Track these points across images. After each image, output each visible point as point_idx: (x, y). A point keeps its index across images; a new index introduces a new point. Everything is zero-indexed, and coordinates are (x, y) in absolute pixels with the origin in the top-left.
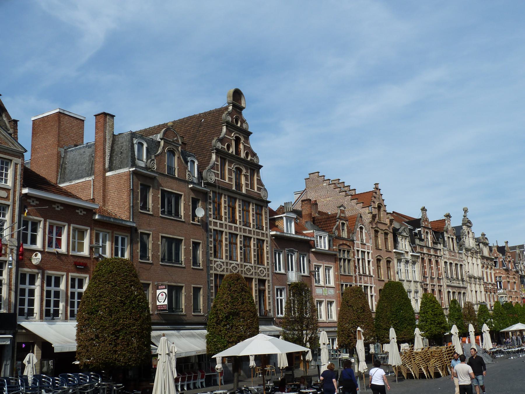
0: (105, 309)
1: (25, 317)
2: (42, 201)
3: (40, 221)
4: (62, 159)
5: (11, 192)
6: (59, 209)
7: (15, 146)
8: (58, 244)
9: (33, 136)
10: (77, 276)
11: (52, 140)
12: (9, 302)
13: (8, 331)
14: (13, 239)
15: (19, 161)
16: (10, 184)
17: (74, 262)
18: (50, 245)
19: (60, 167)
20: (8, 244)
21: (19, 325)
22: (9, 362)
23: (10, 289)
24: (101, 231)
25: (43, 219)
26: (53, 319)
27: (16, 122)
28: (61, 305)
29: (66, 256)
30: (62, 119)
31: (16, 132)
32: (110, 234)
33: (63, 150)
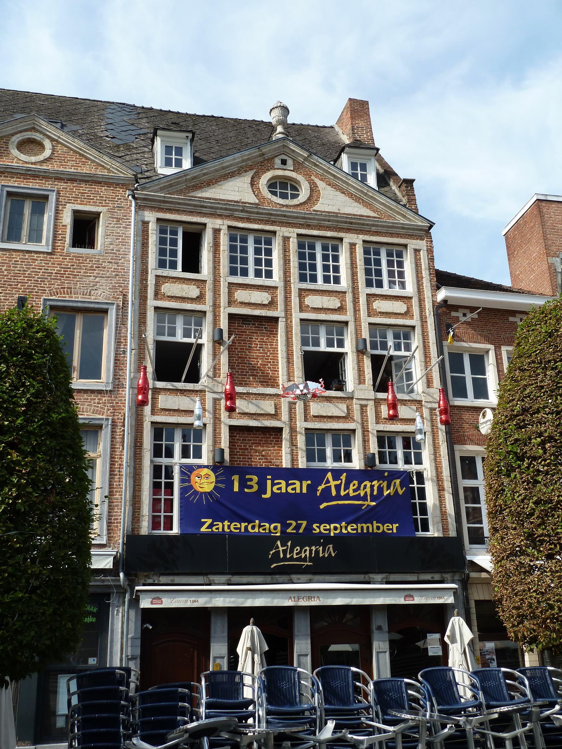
0: (543, 443)
3: (487, 352)
5: (415, 302)
7: (410, 220)
9: (509, 259)
11: (536, 249)
12: (443, 514)
13: (448, 576)
14: (431, 390)
15: (422, 244)
20: (423, 399)
21: (472, 563)
23: (441, 489)
27: (409, 183)
30: (545, 210)
31: (412, 199)
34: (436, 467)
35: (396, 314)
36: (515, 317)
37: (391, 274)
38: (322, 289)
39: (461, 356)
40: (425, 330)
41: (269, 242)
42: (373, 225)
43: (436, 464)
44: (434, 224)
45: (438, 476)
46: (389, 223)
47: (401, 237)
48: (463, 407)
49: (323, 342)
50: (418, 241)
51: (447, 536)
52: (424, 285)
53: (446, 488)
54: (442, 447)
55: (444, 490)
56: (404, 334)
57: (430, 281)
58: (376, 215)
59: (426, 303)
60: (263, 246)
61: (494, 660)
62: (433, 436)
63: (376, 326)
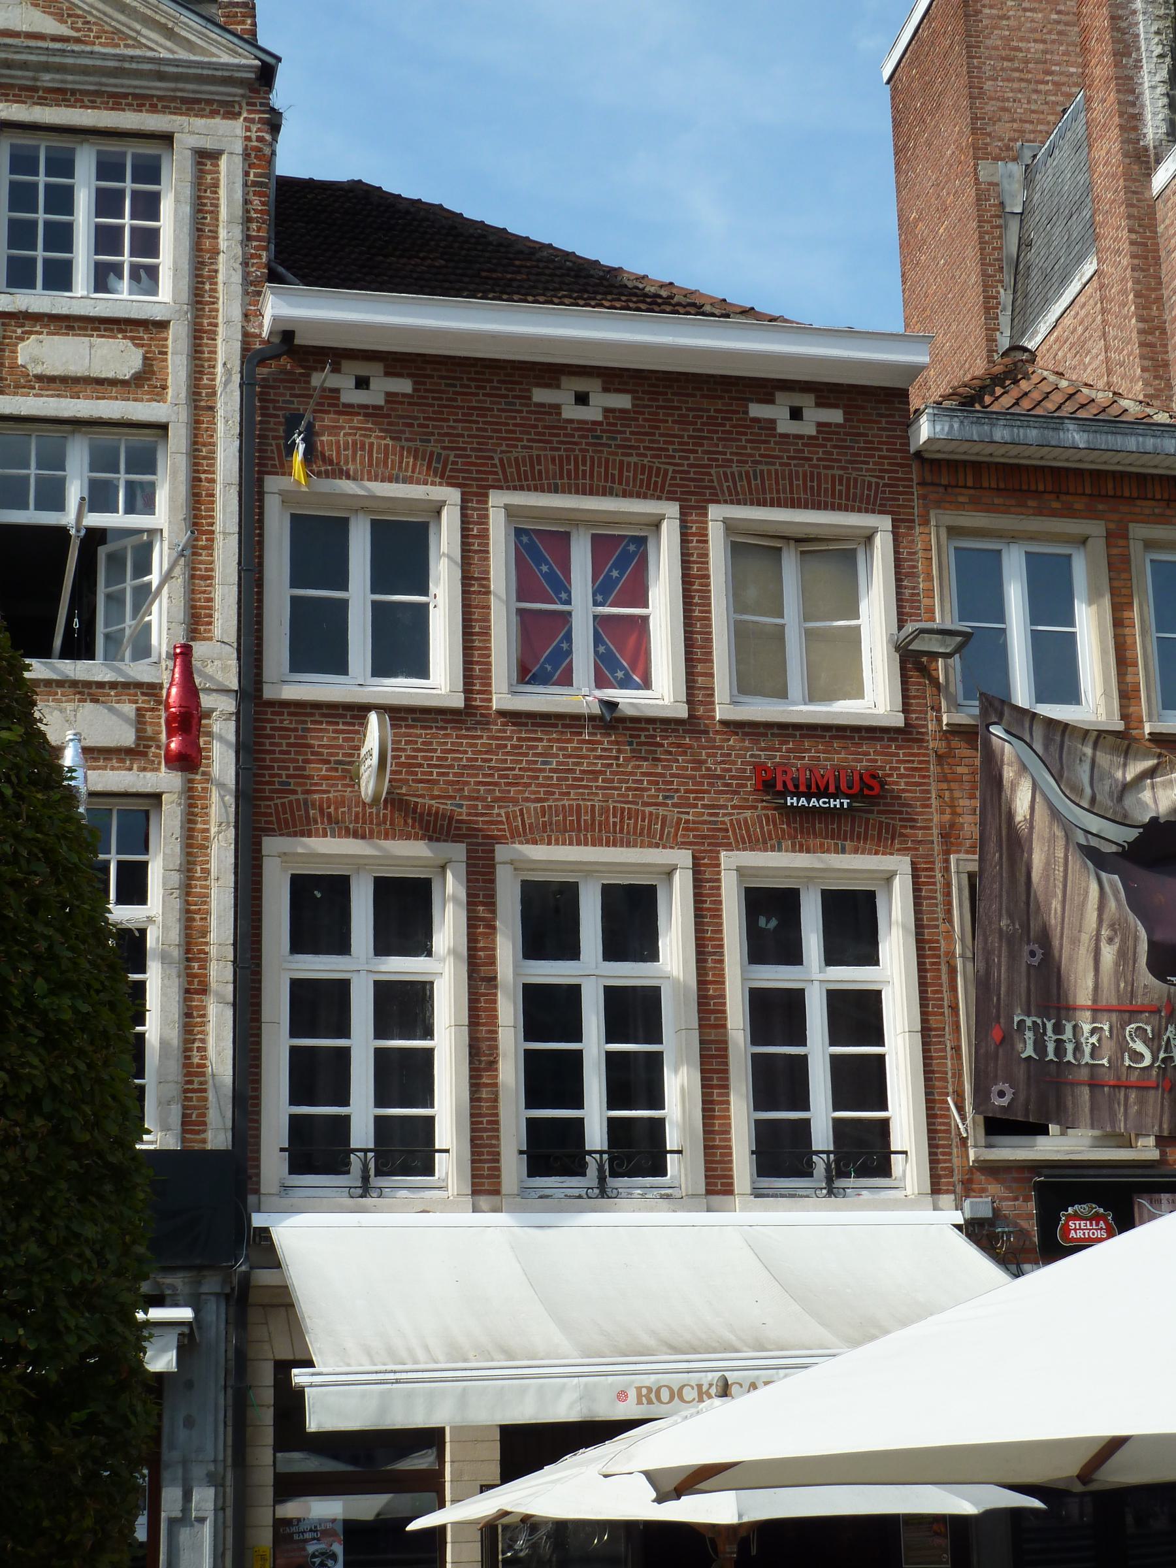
1: (353, 1178)
2: (441, 377)
4: (1014, 226)
6: (591, 413)
7: (190, 46)
8: (623, 649)
10: (810, 875)
12: (192, 1072)
15: (229, 134)
16: (168, 295)
17: (758, 768)
18: (541, 658)
19: (1008, 278)
22: (204, 1498)
23: (193, 988)
24: (1013, 537)
25: (452, 495)
26: (366, 1189)
28: (680, 1084)
29: (692, 725)
32: (1098, 546)
33: (1017, 169)
34: (188, 911)
35: (100, 382)
36: (558, 387)
37: (107, 239)
38: (93, 312)
39: (340, 527)
40: (205, 438)
41: (150, 172)
42: (46, 67)
43: (188, 903)
44: (279, 59)
45: (188, 944)
46: (104, 56)
47: (153, 109)
48: (317, 706)
49: (75, 492)
50: (217, 121)
51: (197, 1146)
52: (221, 278)
53: (213, 985)
54: (215, 846)
55: (204, 991)
56: (130, 453)
57: (245, 264)
58: (64, 30)
59: (219, 341)
60: (129, 186)
61: (333, 1557)
62: (191, 806)
63: (28, 426)
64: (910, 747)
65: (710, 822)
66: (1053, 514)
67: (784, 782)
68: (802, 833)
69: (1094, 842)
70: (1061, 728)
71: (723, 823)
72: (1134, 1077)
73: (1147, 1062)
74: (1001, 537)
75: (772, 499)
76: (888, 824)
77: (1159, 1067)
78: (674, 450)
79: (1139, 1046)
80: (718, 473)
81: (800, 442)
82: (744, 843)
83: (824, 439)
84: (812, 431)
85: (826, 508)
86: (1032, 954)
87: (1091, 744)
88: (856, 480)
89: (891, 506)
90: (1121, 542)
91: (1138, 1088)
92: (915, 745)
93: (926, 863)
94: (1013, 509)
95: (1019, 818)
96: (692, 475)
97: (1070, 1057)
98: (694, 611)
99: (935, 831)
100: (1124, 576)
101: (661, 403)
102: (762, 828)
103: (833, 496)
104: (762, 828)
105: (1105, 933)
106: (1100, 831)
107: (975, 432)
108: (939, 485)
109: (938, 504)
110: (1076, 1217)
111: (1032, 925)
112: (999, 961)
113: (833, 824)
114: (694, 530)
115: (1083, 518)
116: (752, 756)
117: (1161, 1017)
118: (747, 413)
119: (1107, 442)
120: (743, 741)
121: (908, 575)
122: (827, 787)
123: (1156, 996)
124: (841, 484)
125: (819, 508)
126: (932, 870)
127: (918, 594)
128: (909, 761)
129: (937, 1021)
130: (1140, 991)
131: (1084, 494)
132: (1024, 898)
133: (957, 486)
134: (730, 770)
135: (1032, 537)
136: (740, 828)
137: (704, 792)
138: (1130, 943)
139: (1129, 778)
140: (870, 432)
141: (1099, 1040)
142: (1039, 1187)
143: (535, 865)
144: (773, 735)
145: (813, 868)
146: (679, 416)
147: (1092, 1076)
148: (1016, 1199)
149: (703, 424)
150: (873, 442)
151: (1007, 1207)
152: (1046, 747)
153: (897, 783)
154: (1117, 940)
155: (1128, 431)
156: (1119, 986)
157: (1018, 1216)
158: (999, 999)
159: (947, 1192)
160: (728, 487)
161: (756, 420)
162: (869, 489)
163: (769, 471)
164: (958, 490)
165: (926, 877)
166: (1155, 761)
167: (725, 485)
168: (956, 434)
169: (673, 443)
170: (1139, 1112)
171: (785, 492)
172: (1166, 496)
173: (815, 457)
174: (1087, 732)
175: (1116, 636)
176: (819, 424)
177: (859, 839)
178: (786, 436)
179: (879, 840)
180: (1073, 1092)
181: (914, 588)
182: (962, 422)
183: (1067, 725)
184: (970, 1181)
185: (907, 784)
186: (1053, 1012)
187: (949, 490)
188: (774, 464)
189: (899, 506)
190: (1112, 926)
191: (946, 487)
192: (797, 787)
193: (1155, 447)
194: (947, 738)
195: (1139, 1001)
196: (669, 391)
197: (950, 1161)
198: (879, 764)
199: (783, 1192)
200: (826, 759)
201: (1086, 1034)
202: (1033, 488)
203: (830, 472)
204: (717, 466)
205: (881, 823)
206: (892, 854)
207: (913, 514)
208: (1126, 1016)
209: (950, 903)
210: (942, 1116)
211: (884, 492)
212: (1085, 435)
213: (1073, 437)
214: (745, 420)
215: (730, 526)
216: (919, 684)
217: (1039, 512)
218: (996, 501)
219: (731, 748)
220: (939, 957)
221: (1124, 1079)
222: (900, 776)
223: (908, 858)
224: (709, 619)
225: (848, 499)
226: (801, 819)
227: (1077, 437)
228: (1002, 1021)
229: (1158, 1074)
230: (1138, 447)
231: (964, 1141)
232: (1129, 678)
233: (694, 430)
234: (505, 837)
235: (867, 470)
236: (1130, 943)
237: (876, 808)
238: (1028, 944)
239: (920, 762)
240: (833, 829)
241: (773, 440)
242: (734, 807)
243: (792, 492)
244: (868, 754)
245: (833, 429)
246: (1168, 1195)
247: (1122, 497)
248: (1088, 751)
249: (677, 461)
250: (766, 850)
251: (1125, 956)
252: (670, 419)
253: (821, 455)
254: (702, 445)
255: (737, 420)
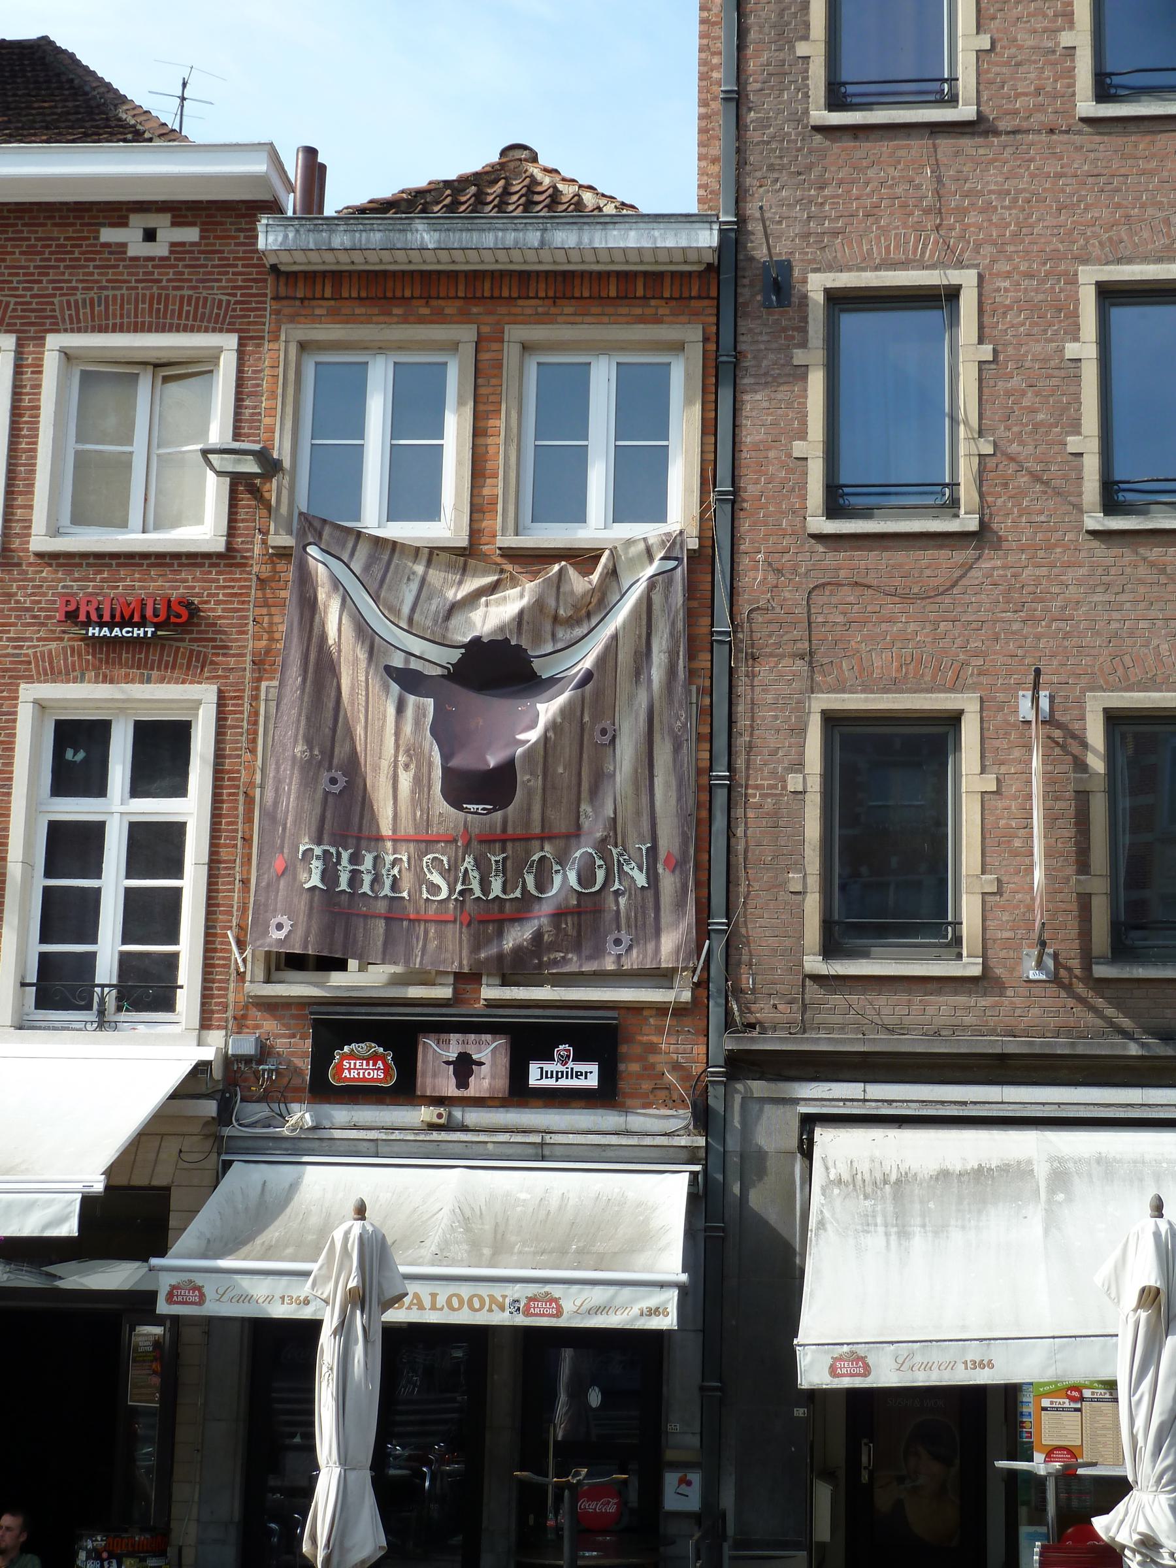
10: (123, 707)
24: (381, 348)
64: (231, 573)
65: (13, 655)
66: (421, 320)
67: (88, 612)
68: (107, 662)
69: (414, 665)
70: (390, 546)
71: (26, 655)
72: (432, 910)
73: (444, 895)
74: (366, 348)
75: (114, 325)
76: (199, 652)
77: (456, 899)
78: (19, 282)
79: (436, 878)
80: (61, 302)
81: (150, 264)
82: (46, 674)
83: (176, 259)
84: (164, 252)
85: (170, 331)
86: (333, 781)
87: (424, 562)
88: (206, 299)
89: (241, 323)
90: (495, 346)
91: (436, 922)
92: (238, 570)
93: (235, 691)
94: (375, 319)
95: (331, 642)
96: (34, 306)
97: (366, 888)
98: (20, 443)
99: (249, 658)
100: (494, 381)
101: (10, 235)
102: (66, 660)
103: (180, 318)
104: (66, 660)
105: (402, 759)
106: (422, 652)
107: (311, 241)
108: (295, 298)
109: (292, 319)
110: (352, 1056)
111: (336, 753)
112: (289, 789)
113: (140, 653)
114: (30, 361)
115: (362, 323)
116: (64, 587)
117: (457, 847)
118: (97, 238)
119: (460, 240)
120: (57, 572)
121: (250, 395)
122: (132, 616)
123: (452, 825)
124: (189, 304)
125: (163, 331)
126: (240, 698)
127: (260, 414)
128: (229, 587)
129: (228, 853)
130: (436, 820)
131: (457, 297)
132: (330, 723)
133: (314, 299)
134: (39, 602)
135: (401, 347)
136: (43, 661)
137: (11, 625)
138: (425, 769)
139: (459, 596)
140: (226, 249)
141: (400, 872)
142: (317, 1024)
143: (63, 703)
144: (88, 565)
145: (126, 699)
146: (28, 246)
147: (390, 909)
148: (293, 1036)
149: (51, 253)
150: (228, 259)
151: (281, 1045)
152: (367, 568)
153: (213, 610)
154: (413, 766)
155: (485, 226)
156: (415, 814)
157: (293, 1054)
158: (284, 829)
159: (219, 1028)
160: (70, 315)
161: (107, 245)
162: (219, 308)
163: (115, 297)
164: (315, 303)
165: (233, 705)
166: (496, 578)
167: (67, 313)
168: (290, 244)
169: (17, 274)
170: (439, 947)
171: (129, 317)
172: (551, 294)
173: (165, 278)
174: (418, 549)
175: (474, 447)
176: (173, 244)
177: (166, 668)
178: (136, 259)
179: (188, 668)
180: (365, 924)
181: (255, 407)
182: (297, 231)
183: (395, 543)
184: (244, 1017)
185: (224, 610)
186: (352, 841)
187: (306, 303)
188: (120, 288)
189: (249, 323)
190: (407, 751)
191: (302, 300)
192: (101, 616)
193: (516, 242)
194: (272, 562)
195: (434, 830)
196: (20, 222)
197: (225, 996)
198: (197, 590)
199: (57, 1024)
200: (141, 588)
201: (388, 866)
202: (399, 294)
203: (179, 293)
204: (61, 295)
205: (192, 651)
206: (201, 683)
207: (263, 331)
208: (423, 846)
209: (256, 732)
210: (222, 950)
211: (234, 310)
212: (436, 235)
213: (422, 238)
214: (95, 245)
215: (68, 356)
216: (249, 506)
217: (405, 320)
218: (358, 311)
219: (44, 580)
220: (238, 787)
221: (422, 912)
222: (218, 603)
223: (214, 688)
224: (35, 450)
225: (195, 320)
226: (108, 651)
227: (426, 237)
228: (286, 851)
229: (455, 908)
230: (496, 243)
231: (241, 976)
232: (486, 491)
233: (41, 260)
234: (31, 677)
235: (219, 288)
236: (425, 769)
237: (188, 637)
238: (330, 769)
239: (241, 587)
240: (140, 659)
241: (122, 264)
242: (39, 640)
243: (136, 316)
244: (186, 581)
245: (188, 248)
246: (457, 1035)
247: (501, 297)
248: (420, 569)
249: (20, 292)
250: (68, 682)
251: (419, 782)
252: (17, 251)
253: (171, 276)
254: (47, 274)
255: (87, 246)
